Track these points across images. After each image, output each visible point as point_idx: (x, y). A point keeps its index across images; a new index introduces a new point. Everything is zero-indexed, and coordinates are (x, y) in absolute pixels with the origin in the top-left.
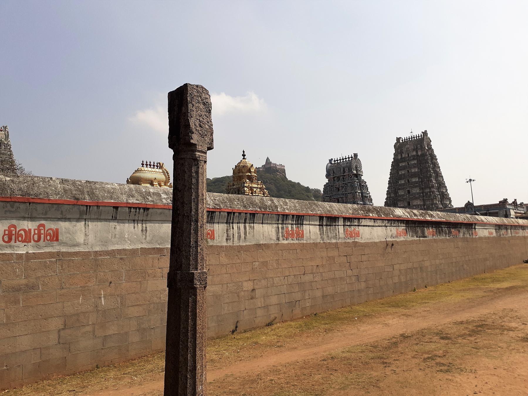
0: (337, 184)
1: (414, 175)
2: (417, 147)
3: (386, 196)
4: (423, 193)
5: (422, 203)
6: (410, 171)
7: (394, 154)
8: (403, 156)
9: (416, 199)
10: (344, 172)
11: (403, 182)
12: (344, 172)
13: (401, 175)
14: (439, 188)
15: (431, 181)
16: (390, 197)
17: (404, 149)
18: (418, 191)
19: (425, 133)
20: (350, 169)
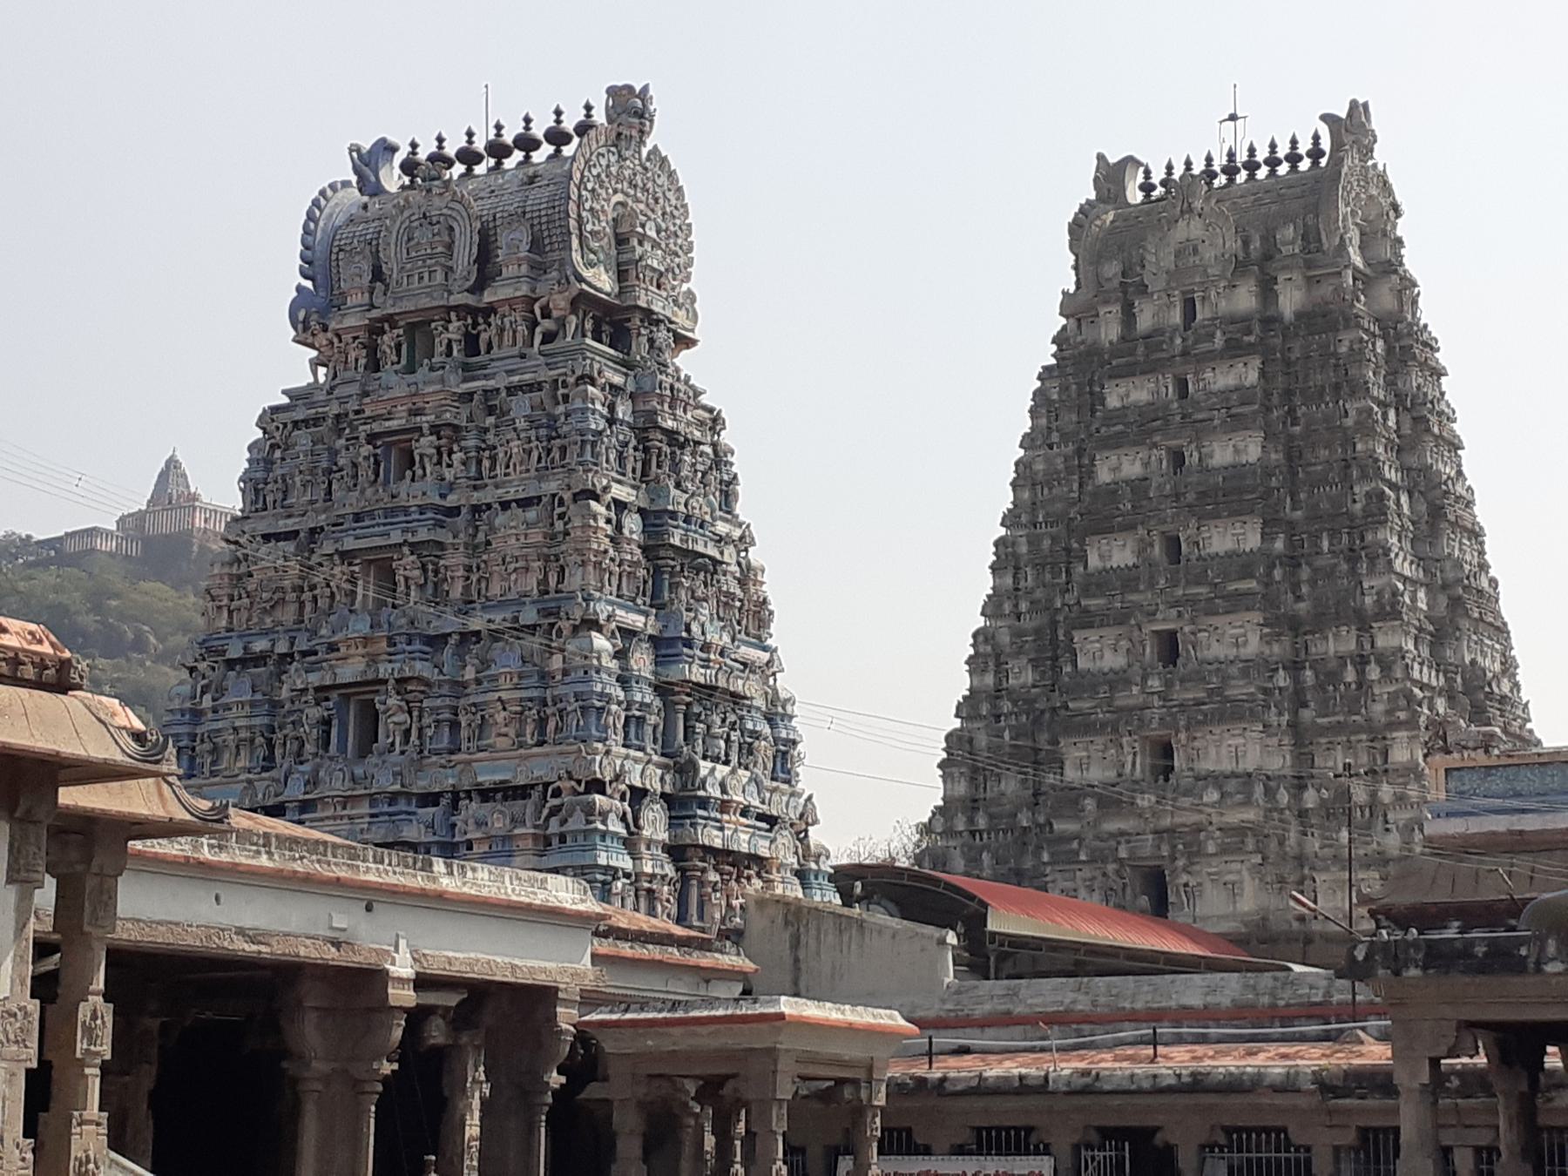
1: (1228, 495)
2: (1269, 238)
6: (1192, 458)
10: (486, 267)
11: (1118, 553)
12: (486, 267)
14: (1440, 635)
15: (1380, 557)
17: (1159, 259)
19: (1352, 128)
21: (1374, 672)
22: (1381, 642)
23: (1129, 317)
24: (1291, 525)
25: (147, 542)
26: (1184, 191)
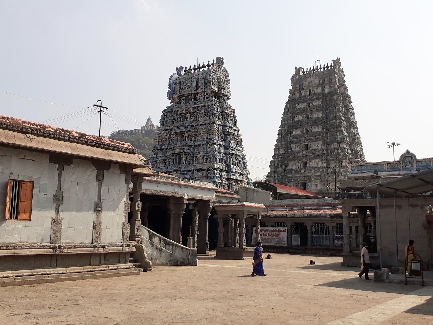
0: (185, 107)
1: (316, 122)
3: (273, 153)
4: (327, 150)
5: (324, 165)
6: (310, 116)
7: (291, 92)
8: (303, 94)
9: (317, 158)
11: (299, 132)
13: (297, 122)
14: (351, 145)
16: (279, 154)
17: (305, 84)
18: (320, 147)
19: (337, 62)
20: (207, 83)
21: (340, 151)
22: (341, 146)
23: (300, 93)
24: (327, 127)
25: (145, 131)
26: (309, 73)
